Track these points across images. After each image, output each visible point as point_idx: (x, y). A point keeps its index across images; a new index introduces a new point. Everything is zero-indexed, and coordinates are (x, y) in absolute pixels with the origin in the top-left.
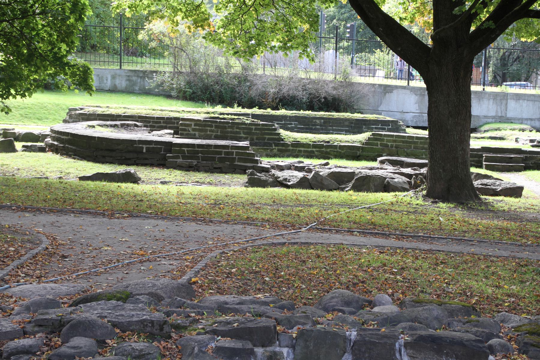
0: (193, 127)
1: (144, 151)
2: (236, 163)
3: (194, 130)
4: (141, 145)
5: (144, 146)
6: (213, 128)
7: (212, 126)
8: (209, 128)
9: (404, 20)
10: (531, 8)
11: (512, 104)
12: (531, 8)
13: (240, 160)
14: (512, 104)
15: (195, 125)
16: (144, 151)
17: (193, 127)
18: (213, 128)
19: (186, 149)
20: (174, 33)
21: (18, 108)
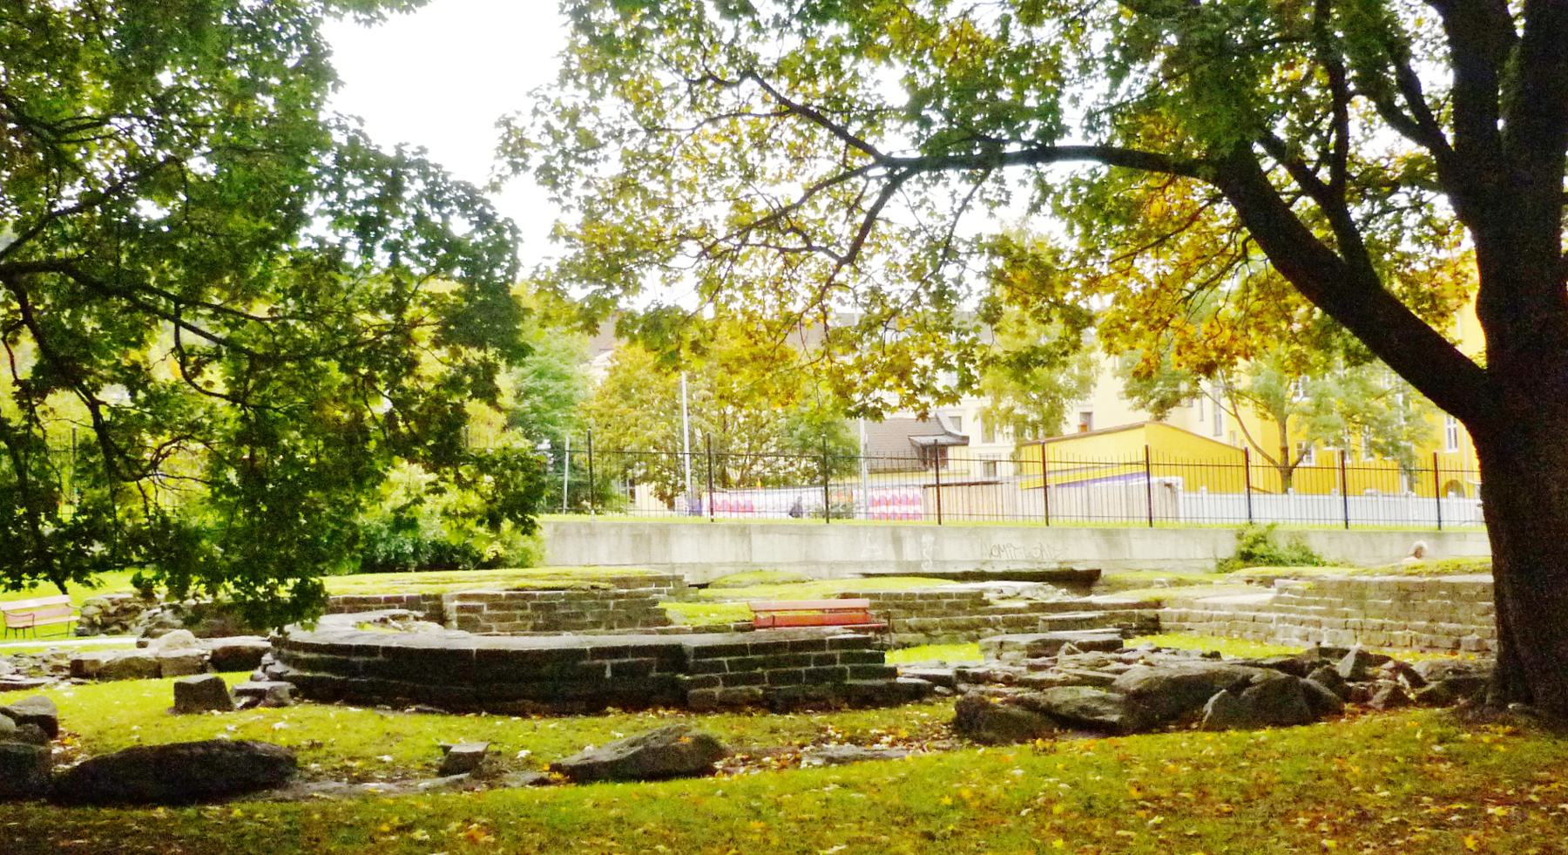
0: (485, 611)
1: (608, 674)
2: (849, 682)
3: (489, 618)
4: (598, 661)
5: (608, 662)
6: (529, 611)
7: (524, 608)
8: (519, 612)
9: (1015, 252)
10: (1481, 362)
11: (757, 540)
12: (1481, 362)
13: (856, 673)
14: (757, 540)
15: (491, 607)
16: (608, 674)
17: (485, 611)
18: (529, 611)
19: (725, 659)
20: (548, 175)
21: (548, 523)
